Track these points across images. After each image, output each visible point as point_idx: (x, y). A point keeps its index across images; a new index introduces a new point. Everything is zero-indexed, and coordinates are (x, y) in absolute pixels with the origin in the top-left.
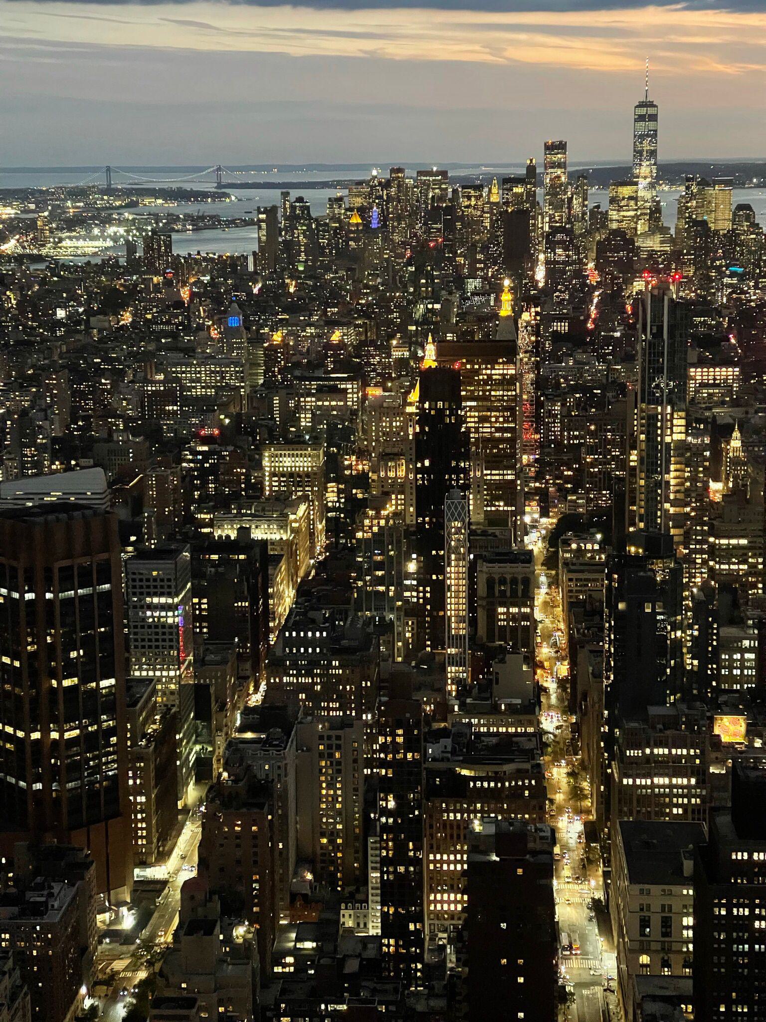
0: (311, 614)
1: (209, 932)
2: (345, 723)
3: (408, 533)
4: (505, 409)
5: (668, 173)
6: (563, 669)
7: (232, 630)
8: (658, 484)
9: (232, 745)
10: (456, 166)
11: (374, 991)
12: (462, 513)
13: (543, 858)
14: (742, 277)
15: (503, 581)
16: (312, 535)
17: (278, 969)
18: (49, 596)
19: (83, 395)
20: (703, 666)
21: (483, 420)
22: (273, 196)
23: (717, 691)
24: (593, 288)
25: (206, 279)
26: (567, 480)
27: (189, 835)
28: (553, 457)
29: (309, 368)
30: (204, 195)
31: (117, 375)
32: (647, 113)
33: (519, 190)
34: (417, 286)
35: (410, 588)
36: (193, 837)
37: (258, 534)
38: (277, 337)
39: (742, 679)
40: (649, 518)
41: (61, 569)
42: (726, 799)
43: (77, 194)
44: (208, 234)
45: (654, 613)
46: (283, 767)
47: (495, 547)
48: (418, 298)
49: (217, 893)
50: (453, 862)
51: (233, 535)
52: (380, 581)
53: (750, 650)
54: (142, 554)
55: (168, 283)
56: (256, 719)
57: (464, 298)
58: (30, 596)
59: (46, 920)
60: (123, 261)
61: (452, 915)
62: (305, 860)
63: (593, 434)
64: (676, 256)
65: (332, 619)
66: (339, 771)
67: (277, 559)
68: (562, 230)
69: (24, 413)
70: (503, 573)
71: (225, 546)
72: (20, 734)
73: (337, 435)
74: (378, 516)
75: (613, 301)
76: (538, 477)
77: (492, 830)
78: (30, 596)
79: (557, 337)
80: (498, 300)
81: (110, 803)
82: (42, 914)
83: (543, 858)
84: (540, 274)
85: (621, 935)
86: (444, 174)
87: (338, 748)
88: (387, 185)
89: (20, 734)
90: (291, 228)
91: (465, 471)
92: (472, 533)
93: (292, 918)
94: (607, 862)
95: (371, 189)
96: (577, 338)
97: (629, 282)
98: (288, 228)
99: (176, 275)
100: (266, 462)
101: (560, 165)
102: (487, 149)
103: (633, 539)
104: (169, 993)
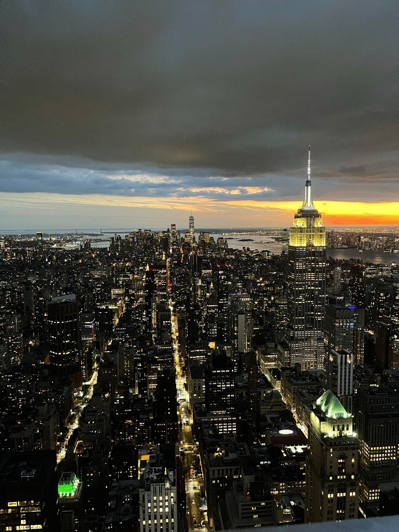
0: (122, 324)
1: (100, 396)
2: (130, 348)
3: (143, 306)
4: (164, 279)
5: (196, 231)
6: (177, 334)
7: (105, 329)
8: (196, 294)
9: (105, 354)
10: (153, 229)
11: (137, 406)
12: (155, 301)
13: (173, 375)
14: (212, 252)
15: (164, 316)
16: (122, 308)
17: (115, 403)
18: (63, 322)
19: (70, 278)
20: (206, 332)
21: (159, 281)
22: (113, 235)
23: (209, 337)
24: (182, 254)
25: (98, 252)
26: (178, 294)
27: (95, 374)
28: (174, 289)
29: (122, 271)
30: (97, 235)
31: (78, 274)
32: (192, 219)
33: (166, 234)
34: (145, 254)
35: (144, 318)
36: (96, 375)
37: (110, 307)
38: (114, 265)
39: (214, 334)
40: (195, 301)
41: (65, 316)
42: (211, 360)
43: (69, 235)
44: (99, 243)
45: (196, 321)
46: (116, 359)
47: (162, 308)
48: (145, 256)
49: (100, 388)
50: (154, 377)
51: (105, 308)
52: (137, 317)
53: (216, 328)
54: (84, 312)
55: (90, 253)
56: (109, 348)
57: (155, 256)
58: (58, 322)
59: (62, 395)
60: (79, 249)
61: (154, 389)
62: (121, 379)
63: (182, 284)
64: (198, 248)
65: (127, 325)
66: (128, 359)
67: (115, 313)
68: (175, 242)
69: (57, 282)
70: (164, 314)
71: (103, 310)
72: (56, 354)
73: (128, 285)
74: (137, 303)
75: (186, 256)
76: (171, 293)
77: (162, 369)
78: (58, 322)
79: (175, 264)
80: (162, 257)
81: (78, 367)
82: (61, 394)
83: (173, 375)
84: (171, 251)
85: (190, 390)
86: (150, 230)
87: (128, 354)
88: (138, 233)
89: (56, 354)
90: (117, 242)
91: (156, 292)
92: (157, 306)
93: (118, 392)
94: (187, 375)
95: (133, 233)
96: (179, 265)
97: (189, 253)
98: (116, 242)
99: (92, 252)
100: (112, 292)
101: (175, 229)
102: (158, 226)
103: (191, 306)
104: (91, 410)
